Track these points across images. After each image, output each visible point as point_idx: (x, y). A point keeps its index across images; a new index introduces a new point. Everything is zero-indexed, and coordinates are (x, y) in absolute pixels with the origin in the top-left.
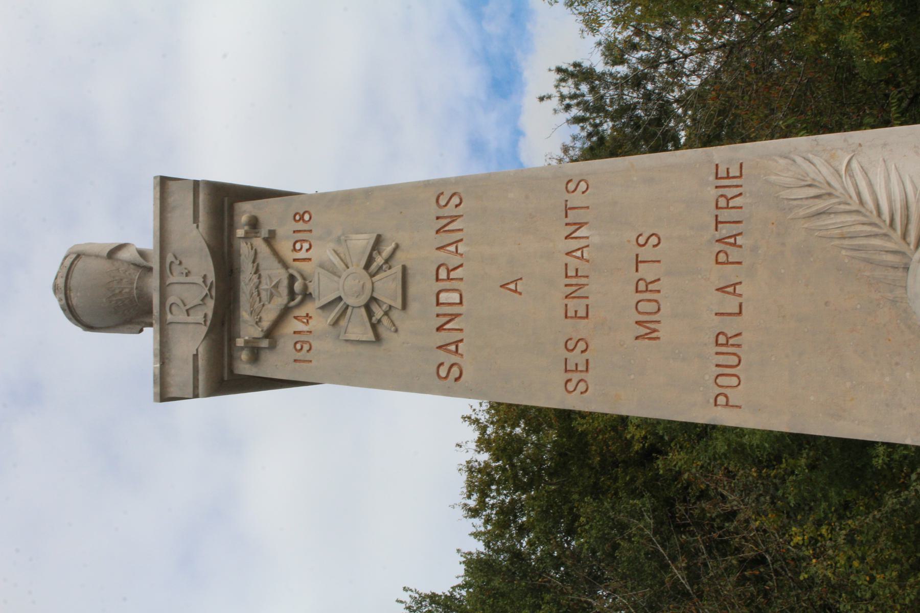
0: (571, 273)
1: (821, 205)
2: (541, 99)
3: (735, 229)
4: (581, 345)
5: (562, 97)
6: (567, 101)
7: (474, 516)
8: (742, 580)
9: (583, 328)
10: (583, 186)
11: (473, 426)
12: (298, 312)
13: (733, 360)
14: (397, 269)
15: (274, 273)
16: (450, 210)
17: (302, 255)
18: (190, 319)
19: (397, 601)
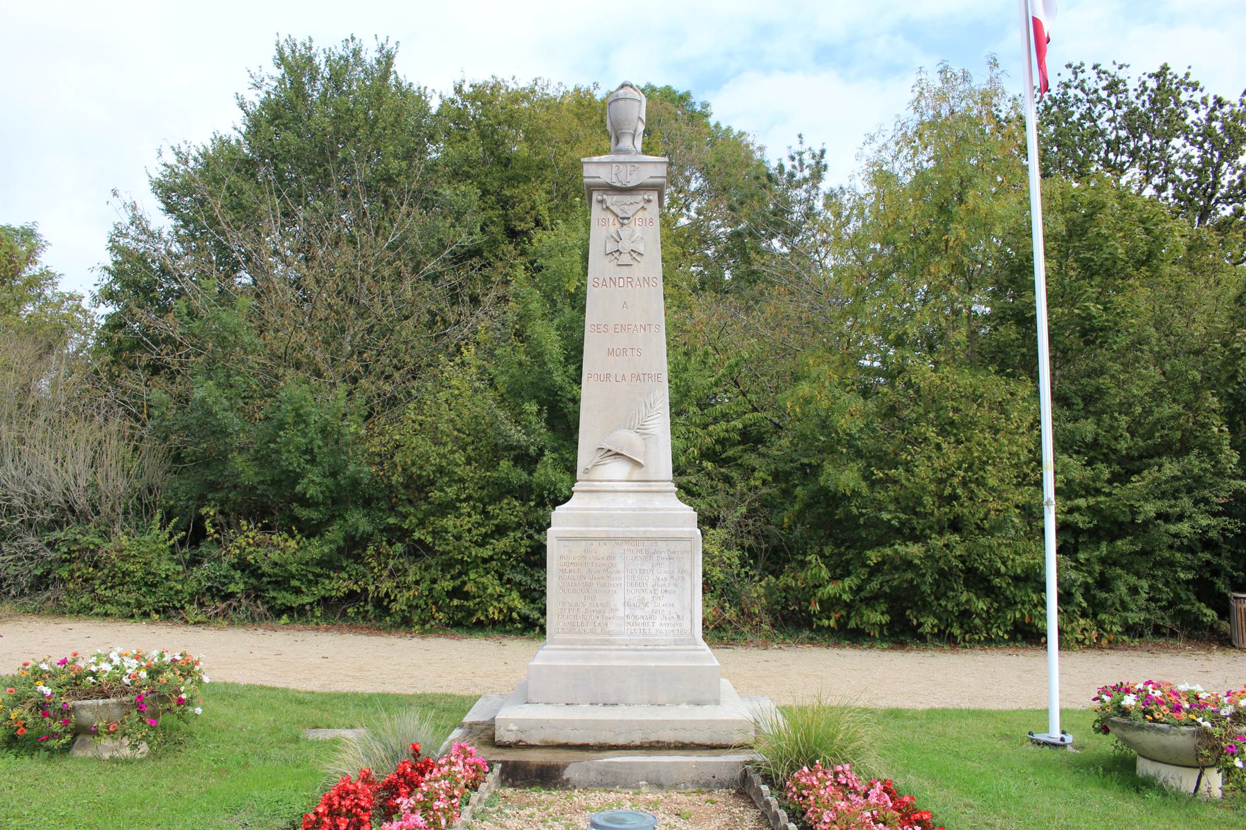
1: (648, 405)
2: (800, 136)
5: (800, 154)
6: (797, 158)
7: (455, 89)
11: (532, 83)
14: (631, 263)
15: (630, 211)
16: (651, 282)
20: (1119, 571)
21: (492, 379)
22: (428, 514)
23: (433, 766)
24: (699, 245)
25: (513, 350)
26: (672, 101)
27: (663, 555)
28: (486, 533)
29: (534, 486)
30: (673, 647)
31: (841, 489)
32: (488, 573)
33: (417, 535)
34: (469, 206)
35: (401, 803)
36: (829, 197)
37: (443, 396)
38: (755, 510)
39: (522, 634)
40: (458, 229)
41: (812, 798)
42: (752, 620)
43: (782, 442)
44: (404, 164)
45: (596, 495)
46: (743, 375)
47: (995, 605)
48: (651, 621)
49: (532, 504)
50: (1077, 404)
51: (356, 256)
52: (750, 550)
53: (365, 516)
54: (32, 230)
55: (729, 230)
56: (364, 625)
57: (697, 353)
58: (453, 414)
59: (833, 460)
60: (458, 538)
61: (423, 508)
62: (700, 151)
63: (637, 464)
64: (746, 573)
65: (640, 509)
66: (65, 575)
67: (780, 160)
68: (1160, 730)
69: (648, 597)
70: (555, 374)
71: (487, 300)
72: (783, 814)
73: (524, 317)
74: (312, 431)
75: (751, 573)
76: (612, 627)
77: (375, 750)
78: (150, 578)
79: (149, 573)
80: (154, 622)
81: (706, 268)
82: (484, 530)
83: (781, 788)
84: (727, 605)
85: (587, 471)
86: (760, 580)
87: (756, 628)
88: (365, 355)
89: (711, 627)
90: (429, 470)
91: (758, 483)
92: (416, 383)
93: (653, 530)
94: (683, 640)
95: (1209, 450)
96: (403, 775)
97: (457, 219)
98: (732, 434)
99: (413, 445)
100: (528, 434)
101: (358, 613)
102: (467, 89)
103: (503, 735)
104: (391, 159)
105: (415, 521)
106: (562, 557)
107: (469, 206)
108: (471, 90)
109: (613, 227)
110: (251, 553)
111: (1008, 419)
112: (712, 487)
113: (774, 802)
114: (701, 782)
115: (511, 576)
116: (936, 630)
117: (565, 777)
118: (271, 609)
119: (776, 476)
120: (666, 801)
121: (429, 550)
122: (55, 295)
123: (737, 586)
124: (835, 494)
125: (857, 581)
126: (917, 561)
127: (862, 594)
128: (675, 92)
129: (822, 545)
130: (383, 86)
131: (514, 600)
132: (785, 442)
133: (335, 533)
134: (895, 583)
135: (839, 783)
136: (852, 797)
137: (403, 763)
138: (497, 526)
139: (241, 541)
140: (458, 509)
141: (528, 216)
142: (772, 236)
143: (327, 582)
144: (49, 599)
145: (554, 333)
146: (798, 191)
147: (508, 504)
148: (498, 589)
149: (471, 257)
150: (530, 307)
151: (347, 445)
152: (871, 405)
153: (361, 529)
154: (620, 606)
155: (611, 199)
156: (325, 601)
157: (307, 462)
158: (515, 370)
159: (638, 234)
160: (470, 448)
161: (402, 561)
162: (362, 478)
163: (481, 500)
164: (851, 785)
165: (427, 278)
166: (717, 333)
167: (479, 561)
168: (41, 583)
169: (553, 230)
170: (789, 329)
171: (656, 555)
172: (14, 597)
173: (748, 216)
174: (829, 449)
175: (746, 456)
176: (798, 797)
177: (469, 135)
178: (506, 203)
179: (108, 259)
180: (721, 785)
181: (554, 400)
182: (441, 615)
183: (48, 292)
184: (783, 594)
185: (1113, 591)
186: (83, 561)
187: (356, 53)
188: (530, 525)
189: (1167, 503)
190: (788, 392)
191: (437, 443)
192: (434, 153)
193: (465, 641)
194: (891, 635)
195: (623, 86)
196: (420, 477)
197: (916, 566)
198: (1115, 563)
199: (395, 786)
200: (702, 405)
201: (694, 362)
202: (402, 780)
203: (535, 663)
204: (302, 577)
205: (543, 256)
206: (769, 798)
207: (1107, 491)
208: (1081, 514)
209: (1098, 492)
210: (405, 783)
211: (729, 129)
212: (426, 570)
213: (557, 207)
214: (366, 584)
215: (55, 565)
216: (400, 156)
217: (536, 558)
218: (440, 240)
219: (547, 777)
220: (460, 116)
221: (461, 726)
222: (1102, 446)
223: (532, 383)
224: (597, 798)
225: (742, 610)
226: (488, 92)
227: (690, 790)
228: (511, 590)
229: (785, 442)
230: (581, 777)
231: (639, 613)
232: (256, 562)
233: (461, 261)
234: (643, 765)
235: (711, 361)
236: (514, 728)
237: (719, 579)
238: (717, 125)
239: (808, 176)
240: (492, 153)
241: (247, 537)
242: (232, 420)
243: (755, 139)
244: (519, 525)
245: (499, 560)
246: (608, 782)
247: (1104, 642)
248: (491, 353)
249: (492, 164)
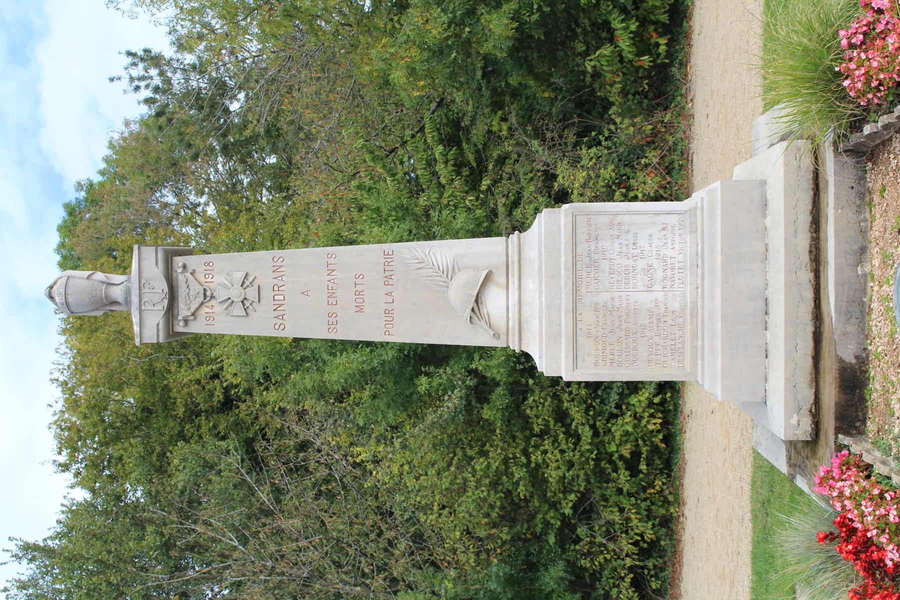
0: (330, 288)
1: (420, 265)
2: (112, 80)
3: (391, 273)
4: (335, 315)
5: (132, 79)
6: (136, 83)
7: (63, 471)
8: (317, 497)
9: (335, 309)
10: (334, 256)
11: (55, 385)
12: (207, 304)
13: (391, 319)
15: (196, 289)
16: (279, 263)
17: (209, 280)
18: (155, 308)
19: (3, 550)
21: (391, 427)
22: (544, 498)
23: (845, 518)
24: (237, 192)
25: (358, 405)
26: (75, 224)
27: (593, 247)
28: (564, 433)
29: (510, 380)
30: (699, 235)
31: (511, 33)
32: (610, 430)
33: (568, 511)
34: (197, 454)
35: (892, 560)
36: (182, 45)
37: (410, 482)
38: (535, 130)
39: (678, 391)
40: (222, 467)
41: (882, 76)
42: (659, 132)
43: (458, 100)
44: (150, 529)
45: (524, 325)
46: (383, 144)
48: (669, 260)
49: (531, 382)
51: (254, 582)
52: (580, 135)
53: (547, 569)
55: (220, 159)
56: (670, 569)
57: (359, 197)
60: (571, 465)
61: (537, 504)
62: (131, 193)
63: (488, 278)
64: (606, 139)
65: (540, 275)
67: (139, 103)
69: (641, 264)
70: (385, 357)
71: (304, 434)
75: (606, 134)
76: (676, 306)
77: (826, 583)
81: (263, 185)
82: (562, 436)
83: (866, 110)
84: (643, 161)
85: (496, 336)
86: (615, 123)
87: (669, 126)
88: (366, 570)
89: (669, 179)
90: (495, 499)
91: (505, 127)
92: (397, 513)
93: (564, 259)
94: (691, 224)
96: (856, 554)
97: (212, 468)
98: (450, 157)
99: (467, 516)
100: (453, 388)
101: (656, 576)
102: (63, 458)
103: (804, 430)
104: (144, 543)
106: (596, 364)
107: (197, 454)
108: (64, 453)
112: (510, 179)
113: (884, 119)
114: (858, 202)
115: (613, 405)
117: (854, 361)
119: (497, 105)
120: (881, 244)
121: (584, 497)
123: (621, 150)
124: (517, 39)
125: (615, 14)
128: (65, 221)
129: (574, 54)
130: (61, 554)
131: (640, 401)
132: (458, 97)
135: (863, 43)
136: (880, 28)
137: (841, 552)
138: (556, 421)
142: (227, 111)
146: (175, 82)
147: (532, 408)
148: (628, 419)
149: (254, 451)
150: (309, 387)
151: (467, 590)
153: (562, 574)
154: (651, 296)
155: (183, 311)
158: (381, 403)
160: (470, 452)
161: (597, 528)
162: (505, 574)
163: (527, 440)
164: (865, 28)
165: (278, 501)
166: (336, 173)
167: (596, 440)
169: (222, 361)
170: (330, 91)
171: (593, 255)
173: (204, 139)
174: (466, 46)
175: (474, 139)
176: (880, 91)
177: (116, 455)
178: (192, 412)
180: (862, 179)
181: (414, 358)
182: (658, 483)
184: (630, 97)
187: (22, 586)
190: (403, 94)
191: (463, 489)
192: (136, 494)
193: (686, 456)
195: (51, 298)
196: (502, 508)
199: (870, 564)
200: (415, 188)
201: (370, 201)
202: (863, 556)
203: (719, 393)
205: (252, 372)
206: (880, 125)
210: (865, 552)
211: (107, 160)
212: (606, 500)
213: (197, 355)
214: (624, 567)
216: (140, 533)
218: (235, 486)
220: (95, 465)
221: (792, 478)
223: (395, 383)
225: (649, 144)
226: (66, 434)
227: (868, 215)
228: (628, 404)
229: (458, 97)
230: (854, 342)
231: (659, 275)
233: (258, 464)
234: (838, 270)
235: (368, 182)
236: (794, 420)
237: (613, 171)
238: (102, 173)
239: (157, 71)
240: (136, 428)
243: (117, 131)
244: (555, 396)
245: (594, 418)
248: (361, 429)
249: (149, 428)
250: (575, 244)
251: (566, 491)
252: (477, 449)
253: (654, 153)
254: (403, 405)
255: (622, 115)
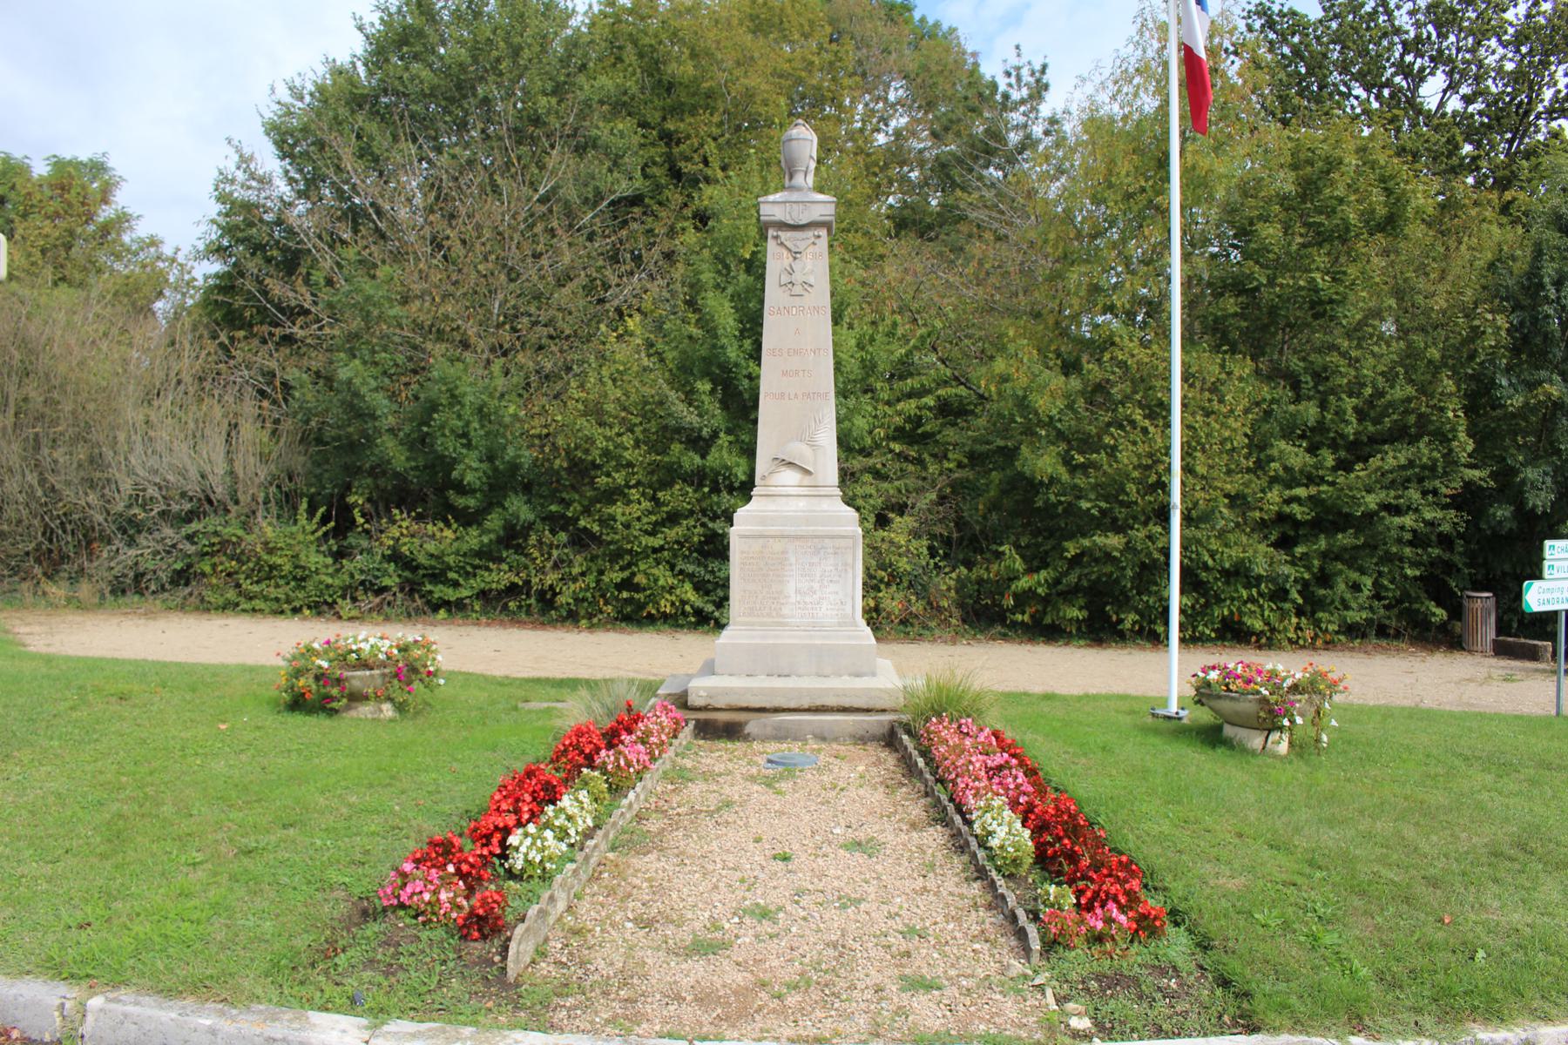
2: (1017, 47)
5: (1018, 69)
6: (1014, 73)
15: (801, 246)
20: (1340, 566)
33: (582, 523)
40: (616, 174)
47: (1202, 601)
49: (706, 490)
50: (1307, 383)
53: (526, 503)
54: (102, 164)
58: (619, 393)
59: (1032, 443)
61: (588, 494)
63: (807, 472)
66: (208, 569)
68: (1232, 699)
69: (816, 586)
72: (915, 753)
73: (695, 287)
74: (467, 412)
76: (785, 611)
78: (299, 573)
79: (296, 567)
80: (305, 618)
82: (654, 518)
85: (764, 478)
86: (951, 572)
87: (946, 622)
93: (820, 529)
95: (1443, 437)
100: (700, 415)
101: (520, 607)
103: (694, 700)
105: (579, 508)
106: (742, 552)
109: (787, 259)
110: (405, 544)
111: (1221, 401)
115: (683, 567)
116: (1137, 627)
118: (428, 603)
122: (132, 241)
126: (1116, 554)
127: (1060, 587)
133: (494, 521)
134: (1093, 577)
139: (395, 532)
140: (625, 495)
141: (695, 156)
143: (486, 574)
144: (191, 594)
145: (727, 304)
148: (670, 581)
152: (1075, 383)
153: (522, 517)
154: (793, 595)
155: (785, 236)
156: (483, 595)
157: (463, 445)
159: (809, 267)
160: (638, 429)
161: (566, 551)
167: (649, 551)
168: (182, 577)
172: (154, 592)
174: (1029, 431)
179: (214, 209)
182: (609, 609)
183: (126, 238)
185: (1331, 588)
186: (225, 554)
188: (704, 512)
189: (1392, 493)
193: (636, 636)
194: (1090, 632)
197: (1115, 558)
198: (1337, 558)
204: (460, 570)
207: (1330, 479)
208: (1300, 505)
209: (1322, 480)
211: (937, 25)
215: (195, 559)
217: (716, 548)
219: (731, 732)
222: (1328, 430)
224: (772, 747)
225: (930, 603)
228: (683, 582)
231: (808, 599)
232: (411, 553)
234: (809, 721)
236: (702, 693)
238: (923, 20)
241: (400, 527)
242: (380, 402)
244: (692, 512)
246: (781, 735)
247: (1319, 643)
250: (833, 537)
251: (602, 522)
252: (641, 437)
253: (921, 608)
254: (683, 366)
255: (958, 579)
